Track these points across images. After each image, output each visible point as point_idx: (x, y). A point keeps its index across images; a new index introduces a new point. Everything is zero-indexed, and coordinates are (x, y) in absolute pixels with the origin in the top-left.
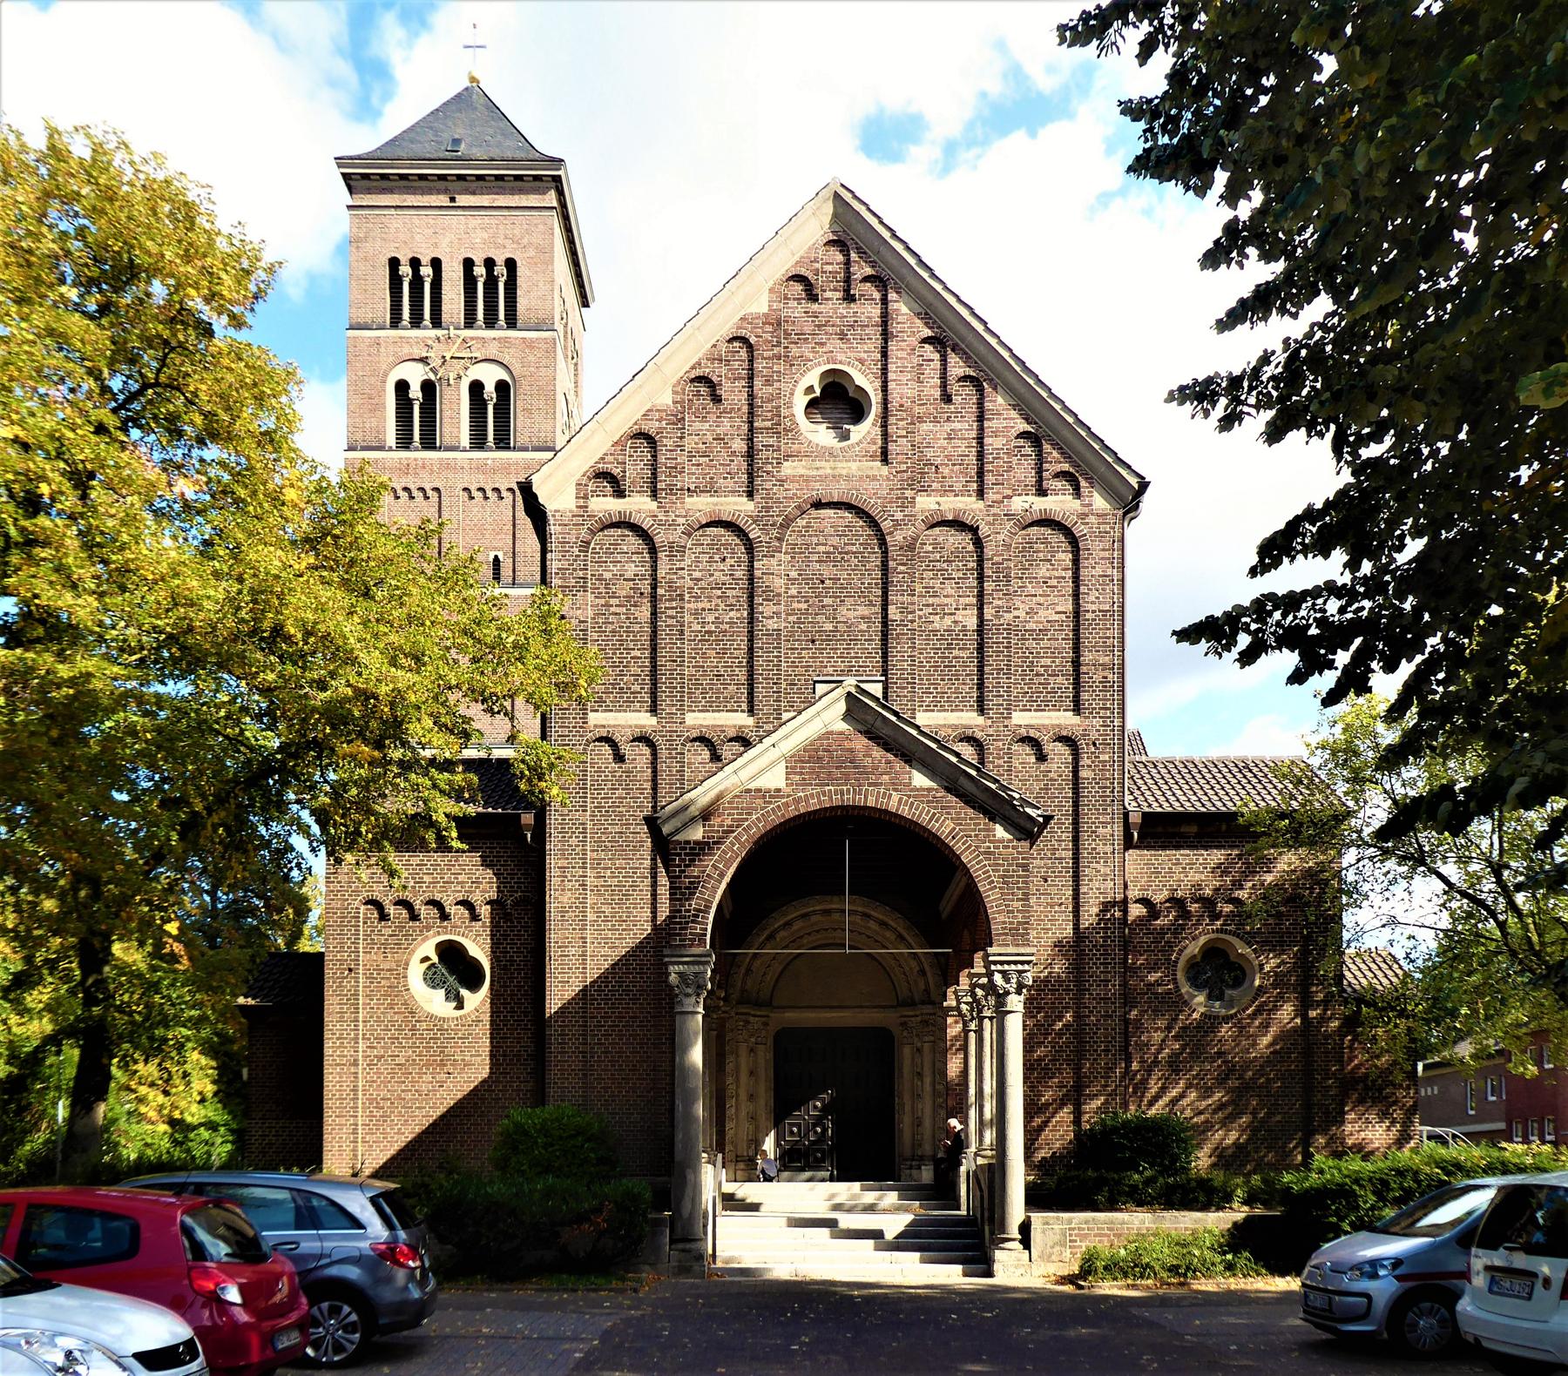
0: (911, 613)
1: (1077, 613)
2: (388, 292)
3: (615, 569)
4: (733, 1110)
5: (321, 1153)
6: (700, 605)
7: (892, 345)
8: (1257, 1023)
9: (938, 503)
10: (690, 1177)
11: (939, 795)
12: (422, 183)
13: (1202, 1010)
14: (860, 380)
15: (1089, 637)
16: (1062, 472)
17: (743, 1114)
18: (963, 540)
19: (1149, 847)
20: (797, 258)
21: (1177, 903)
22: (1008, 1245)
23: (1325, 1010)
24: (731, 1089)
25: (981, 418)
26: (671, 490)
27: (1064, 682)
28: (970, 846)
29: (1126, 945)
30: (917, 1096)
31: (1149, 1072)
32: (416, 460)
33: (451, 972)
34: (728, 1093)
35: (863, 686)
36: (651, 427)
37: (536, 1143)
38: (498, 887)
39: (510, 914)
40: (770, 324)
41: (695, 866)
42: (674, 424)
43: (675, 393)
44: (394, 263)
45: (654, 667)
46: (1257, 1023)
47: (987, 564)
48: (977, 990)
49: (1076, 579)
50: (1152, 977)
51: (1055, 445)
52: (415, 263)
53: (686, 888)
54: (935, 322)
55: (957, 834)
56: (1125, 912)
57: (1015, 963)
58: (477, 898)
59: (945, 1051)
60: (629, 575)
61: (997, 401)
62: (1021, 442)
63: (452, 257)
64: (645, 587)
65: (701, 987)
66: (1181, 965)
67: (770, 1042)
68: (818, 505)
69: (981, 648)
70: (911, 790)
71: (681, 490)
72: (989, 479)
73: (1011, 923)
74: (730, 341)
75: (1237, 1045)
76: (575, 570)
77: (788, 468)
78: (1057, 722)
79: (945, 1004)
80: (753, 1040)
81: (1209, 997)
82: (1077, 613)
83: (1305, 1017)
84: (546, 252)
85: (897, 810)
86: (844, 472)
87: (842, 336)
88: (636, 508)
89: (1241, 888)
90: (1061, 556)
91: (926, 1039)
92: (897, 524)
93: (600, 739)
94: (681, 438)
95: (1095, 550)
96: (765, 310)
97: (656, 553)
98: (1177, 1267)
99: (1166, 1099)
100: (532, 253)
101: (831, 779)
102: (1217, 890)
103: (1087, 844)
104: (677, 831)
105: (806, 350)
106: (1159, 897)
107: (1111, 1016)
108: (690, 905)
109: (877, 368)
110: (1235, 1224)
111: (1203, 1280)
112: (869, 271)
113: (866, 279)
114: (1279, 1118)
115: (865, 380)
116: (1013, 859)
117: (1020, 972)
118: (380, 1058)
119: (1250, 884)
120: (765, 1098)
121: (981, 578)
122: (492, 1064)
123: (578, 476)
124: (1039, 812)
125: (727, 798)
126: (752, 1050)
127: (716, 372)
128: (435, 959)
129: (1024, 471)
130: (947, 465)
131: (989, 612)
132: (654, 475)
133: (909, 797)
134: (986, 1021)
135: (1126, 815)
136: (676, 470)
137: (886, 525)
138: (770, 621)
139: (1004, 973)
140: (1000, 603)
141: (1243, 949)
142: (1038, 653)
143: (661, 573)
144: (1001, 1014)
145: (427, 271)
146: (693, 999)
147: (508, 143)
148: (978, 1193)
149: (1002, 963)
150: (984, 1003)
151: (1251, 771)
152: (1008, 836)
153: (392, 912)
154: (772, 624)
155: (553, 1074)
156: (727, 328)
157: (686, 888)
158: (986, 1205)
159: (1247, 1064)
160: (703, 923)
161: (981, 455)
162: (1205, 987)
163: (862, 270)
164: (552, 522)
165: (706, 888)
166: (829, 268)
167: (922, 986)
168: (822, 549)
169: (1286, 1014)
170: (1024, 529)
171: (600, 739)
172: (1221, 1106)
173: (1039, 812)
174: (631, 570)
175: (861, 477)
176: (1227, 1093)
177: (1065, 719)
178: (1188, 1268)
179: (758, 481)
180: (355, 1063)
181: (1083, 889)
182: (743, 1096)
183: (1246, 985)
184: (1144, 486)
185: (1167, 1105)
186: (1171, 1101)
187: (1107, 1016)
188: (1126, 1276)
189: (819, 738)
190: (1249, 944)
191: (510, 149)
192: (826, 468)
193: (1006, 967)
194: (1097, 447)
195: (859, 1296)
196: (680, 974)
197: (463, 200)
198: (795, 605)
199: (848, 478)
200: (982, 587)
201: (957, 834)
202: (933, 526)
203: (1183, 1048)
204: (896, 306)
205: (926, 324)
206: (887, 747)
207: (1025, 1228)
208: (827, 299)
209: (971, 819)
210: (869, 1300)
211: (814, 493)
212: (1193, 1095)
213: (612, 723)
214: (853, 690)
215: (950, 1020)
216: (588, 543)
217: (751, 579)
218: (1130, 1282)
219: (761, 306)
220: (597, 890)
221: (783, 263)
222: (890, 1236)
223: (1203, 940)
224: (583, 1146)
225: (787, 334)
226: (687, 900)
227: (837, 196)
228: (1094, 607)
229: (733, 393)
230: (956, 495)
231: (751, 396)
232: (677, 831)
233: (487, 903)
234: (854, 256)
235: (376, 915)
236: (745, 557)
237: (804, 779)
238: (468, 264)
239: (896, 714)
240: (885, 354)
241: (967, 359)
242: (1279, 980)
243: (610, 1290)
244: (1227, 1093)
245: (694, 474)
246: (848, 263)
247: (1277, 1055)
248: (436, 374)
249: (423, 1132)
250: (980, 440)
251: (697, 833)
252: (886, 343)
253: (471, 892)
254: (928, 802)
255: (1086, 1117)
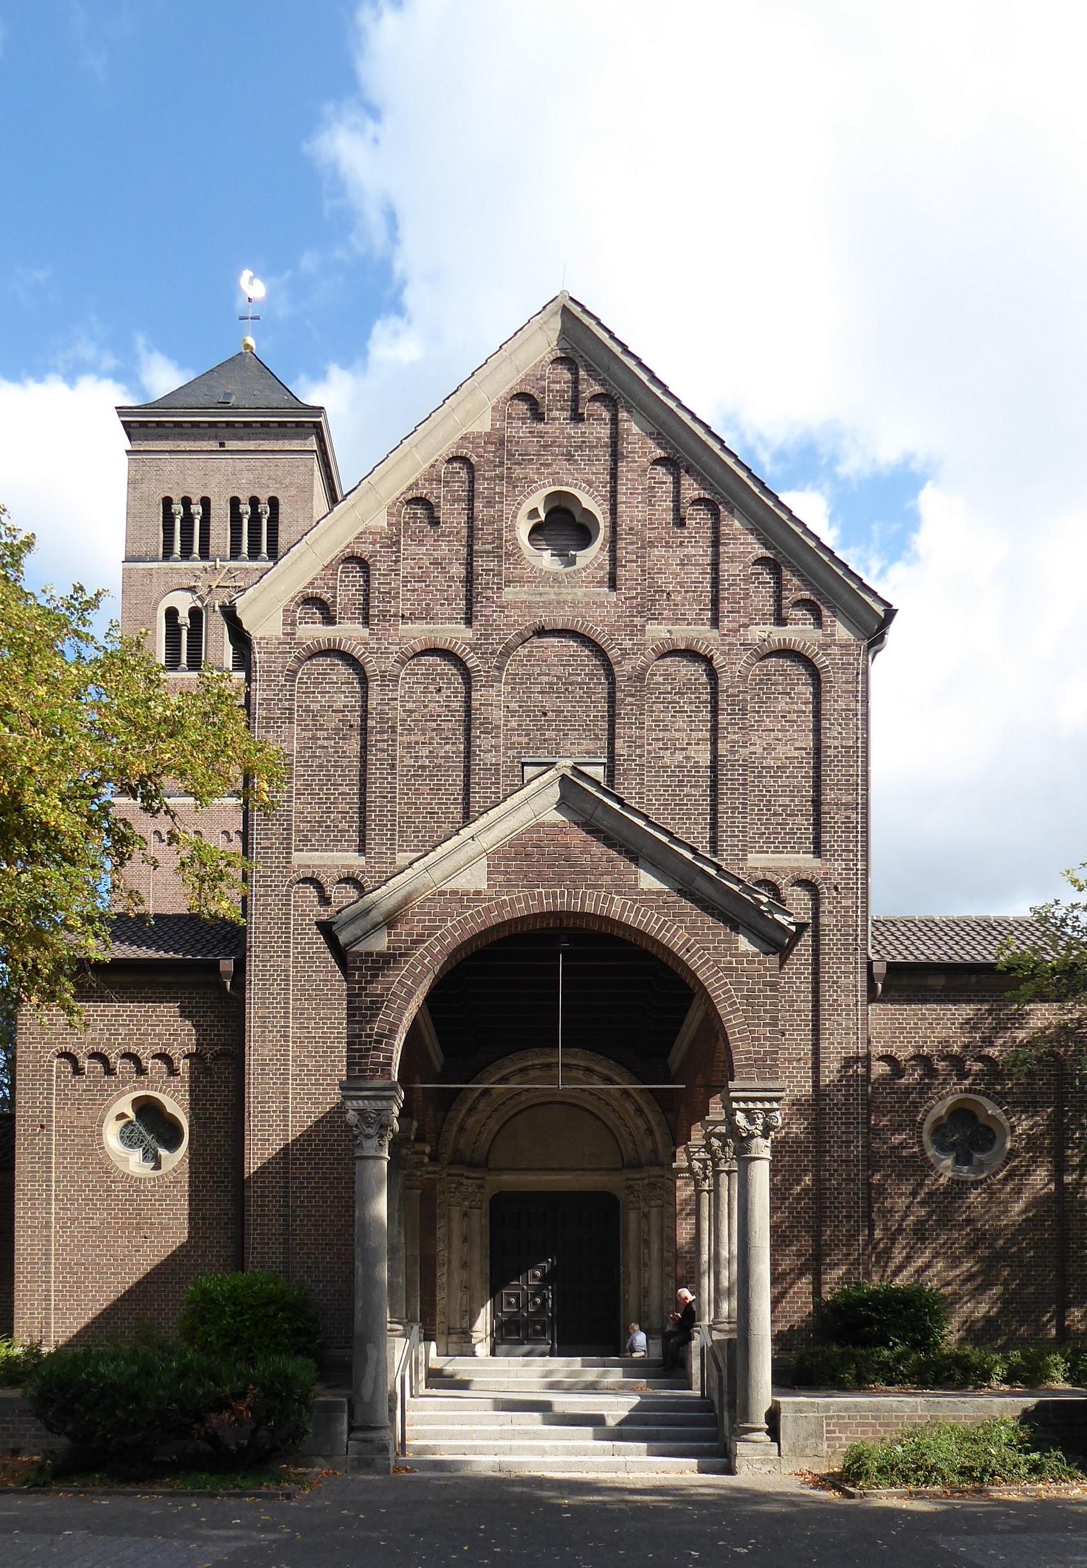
0: (639, 747)
1: (818, 750)
2: (161, 528)
3: (324, 700)
4: (444, 1279)
5: (11, 1318)
6: (413, 738)
7: (622, 467)
8: (1008, 1189)
9: (669, 631)
10: (371, 1352)
11: (670, 899)
12: (195, 430)
13: (949, 1174)
14: (587, 502)
15: (831, 775)
16: (802, 600)
17: (456, 1281)
18: (695, 671)
19: (893, 1001)
20: (522, 375)
21: (923, 1060)
22: (754, 1436)
23: (1081, 1175)
24: (442, 1254)
25: (716, 543)
26: (384, 616)
27: (804, 823)
28: (707, 961)
29: (870, 1105)
30: (643, 1265)
31: (893, 1240)
32: (182, 679)
33: (150, 1132)
34: (439, 1259)
35: (583, 768)
36: (364, 550)
37: (224, 1311)
38: (197, 1040)
39: (210, 1068)
40: (492, 443)
41: (378, 982)
42: (388, 547)
43: (390, 514)
44: (167, 502)
45: (363, 803)
46: (1008, 1189)
47: (722, 697)
48: (713, 1139)
49: (817, 714)
50: (897, 1139)
51: (795, 572)
52: (186, 502)
53: (366, 1009)
54: (668, 442)
55: (693, 946)
56: (868, 1068)
57: (762, 1100)
58: (175, 1052)
59: (674, 1217)
60: (338, 705)
61: (733, 525)
62: (759, 569)
63: (220, 496)
64: (355, 719)
65: (384, 1127)
66: (927, 1126)
67: (486, 1205)
68: (541, 632)
69: (714, 786)
70: (638, 894)
71: (395, 616)
72: (725, 606)
73: (757, 1053)
74: (450, 461)
75: (987, 1212)
76: (280, 700)
77: (509, 594)
78: (796, 865)
79: (674, 1165)
80: (466, 1203)
81: (957, 1161)
82: (818, 750)
83: (1059, 1182)
84: (307, 491)
85: (621, 916)
86: (569, 598)
87: (570, 457)
88: (347, 636)
89: (991, 1044)
90: (803, 689)
91: (653, 1203)
92: (624, 653)
93: (305, 880)
94: (396, 562)
95: (836, 682)
96: (488, 429)
97: (367, 683)
98: (972, 1469)
99: (911, 1269)
100: (293, 491)
101: (541, 879)
102: (966, 1047)
103: (828, 995)
104: (357, 940)
105: (530, 471)
106: (902, 1055)
107: (853, 1180)
108: (372, 1029)
109: (605, 491)
110: (1025, 1411)
111: (1004, 1486)
112: (598, 389)
113: (595, 398)
114: (1032, 1289)
115: (592, 503)
116: (760, 976)
117: (767, 1111)
118: (73, 1220)
119: (1001, 1041)
120: (480, 1266)
121: (715, 711)
122: (191, 1228)
123: (285, 602)
124: (791, 919)
125: (418, 901)
126: (465, 1215)
127: (434, 492)
128: (132, 1115)
129: (762, 598)
130: (679, 592)
131: (723, 747)
132: (367, 601)
133: (635, 901)
134: (723, 1176)
135: (870, 965)
136: (390, 595)
137: (614, 654)
138: (489, 755)
139: (748, 1112)
140: (735, 737)
141: (992, 1110)
142: (777, 791)
143: (372, 703)
144: (745, 1161)
145: (196, 509)
146: (375, 1141)
147: (275, 396)
148: (715, 1373)
149: (745, 1100)
150: (721, 1155)
151: (994, 929)
152: (752, 949)
153: (86, 1065)
154: (490, 758)
155: (252, 1238)
156: (446, 450)
157: (366, 1009)
158: (725, 1388)
159: (998, 1232)
160: (387, 1051)
161: (715, 582)
162: (952, 1150)
163: (591, 388)
164: (256, 650)
165: (391, 1009)
166: (557, 387)
167: (649, 1145)
168: (546, 679)
169: (1040, 1179)
170: (761, 659)
171: (305, 880)
172: (971, 1277)
173: (791, 919)
174: (340, 701)
175: (587, 604)
176: (977, 1262)
177: (805, 861)
178: (984, 1471)
179: (477, 608)
180: (47, 1226)
181: (824, 1044)
182: (456, 1263)
183: (997, 1146)
184: (890, 613)
185: (912, 1276)
186: (916, 1271)
187: (849, 1180)
188: (906, 1480)
189: (528, 831)
190: (1000, 1105)
191: (277, 399)
192: (551, 593)
193: (751, 1105)
194: (840, 573)
195: (570, 1508)
196: (361, 1112)
197: (231, 445)
198: (515, 739)
199: (574, 605)
200: (716, 721)
201: (693, 946)
202: (663, 656)
203: (930, 1214)
204: (626, 425)
205: (659, 445)
206: (609, 841)
207: (773, 1416)
208: (554, 419)
209: (709, 928)
210: (582, 1512)
211: (537, 620)
212: (940, 1265)
213: (317, 863)
214: (569, 773)
215: (679, 1183)
216: (295, 672)
217: (468, 710)
218: (912, 1488)
219: (484, 424)
220: (300, 1043)
221: (507, 380)
222: (611, 1422)
223: (950, 1100)
224: (275, 1315)
225: (511, 455)
226: (368, 1022)
227: (565, 310)
228: (836, 743)
229: (453, 516)
230: (689, 624)
231: (471, 519)
232: (357, 940)
233: (186, 1057)
234: (582, 373)
235: (70, 1069)
236: (461, 688)
237: (509, 880)
238: (235, 502)
239: (620, 801)
240: (614, 475)
241: (703, 483)
242: (1032, 1143)
243: (258, 1496)
244: (977, 1262)
245: (409, 600)
246: (576, 382)
247: (1029, 1225)
248: (203, 602)
249: (118, 1300)
250: (715, 565)
251: (380, 943)
252: (616, 464)
253: (169, 1045)
254: (658, 908)
255: (826, 1288)
